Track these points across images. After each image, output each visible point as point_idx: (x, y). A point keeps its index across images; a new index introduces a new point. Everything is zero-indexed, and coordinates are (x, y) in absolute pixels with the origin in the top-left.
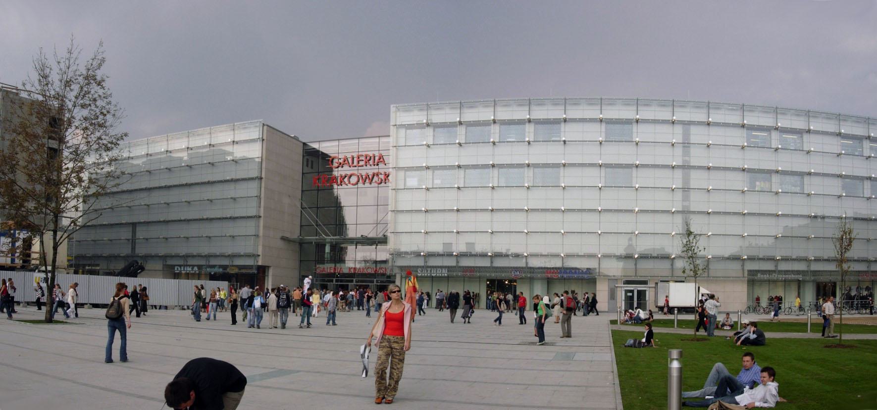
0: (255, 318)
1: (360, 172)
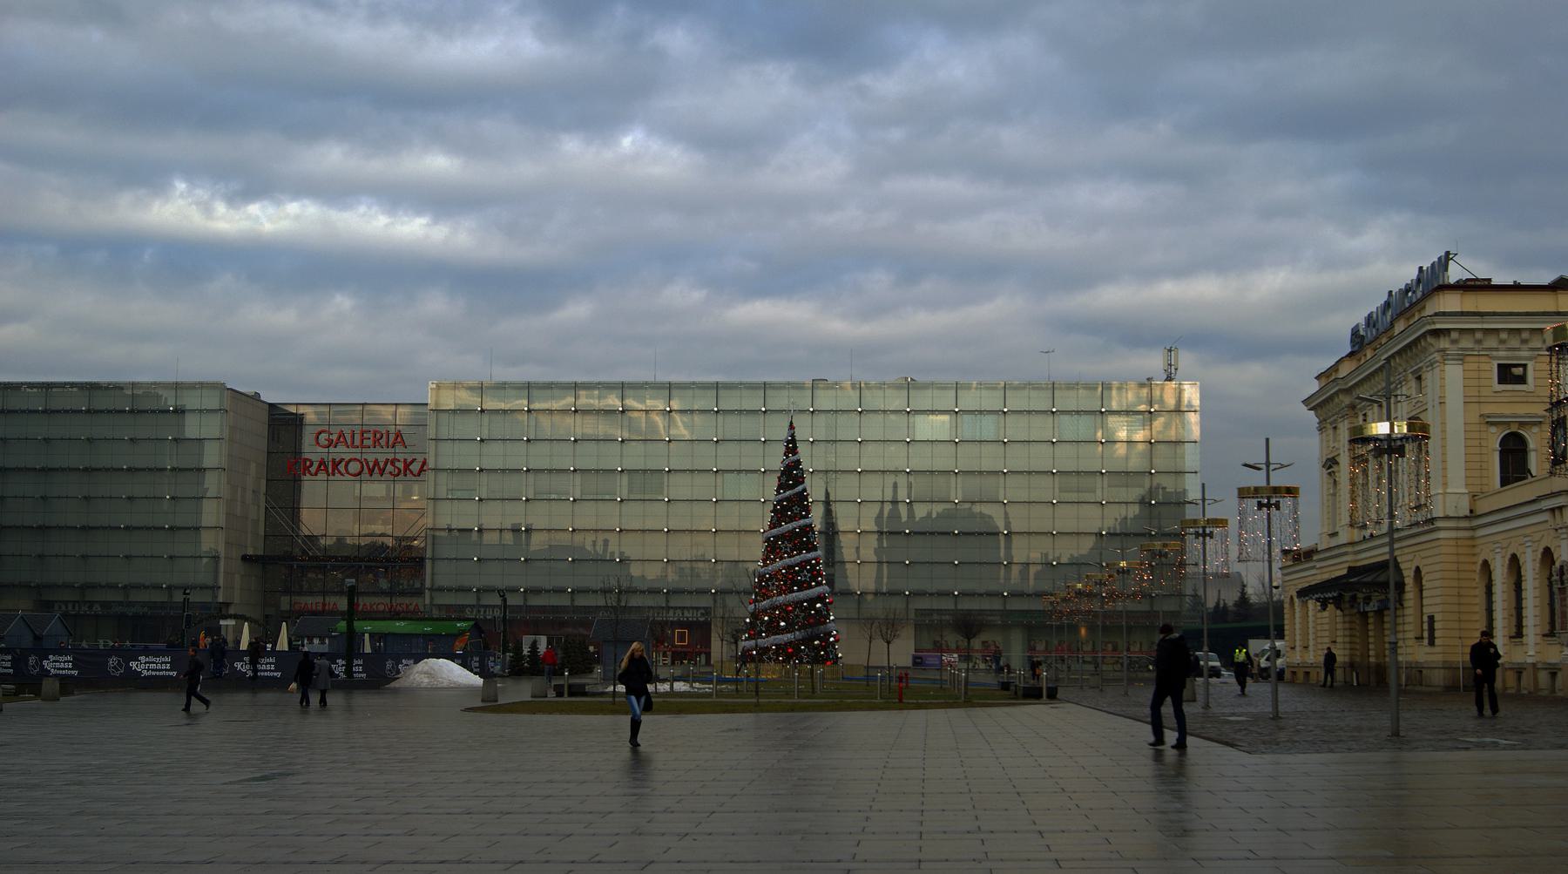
0: (388, 689)
1: (364, 456)
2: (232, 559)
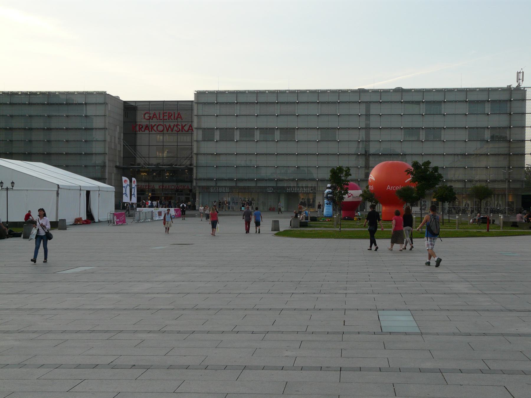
2: (111, 167)
